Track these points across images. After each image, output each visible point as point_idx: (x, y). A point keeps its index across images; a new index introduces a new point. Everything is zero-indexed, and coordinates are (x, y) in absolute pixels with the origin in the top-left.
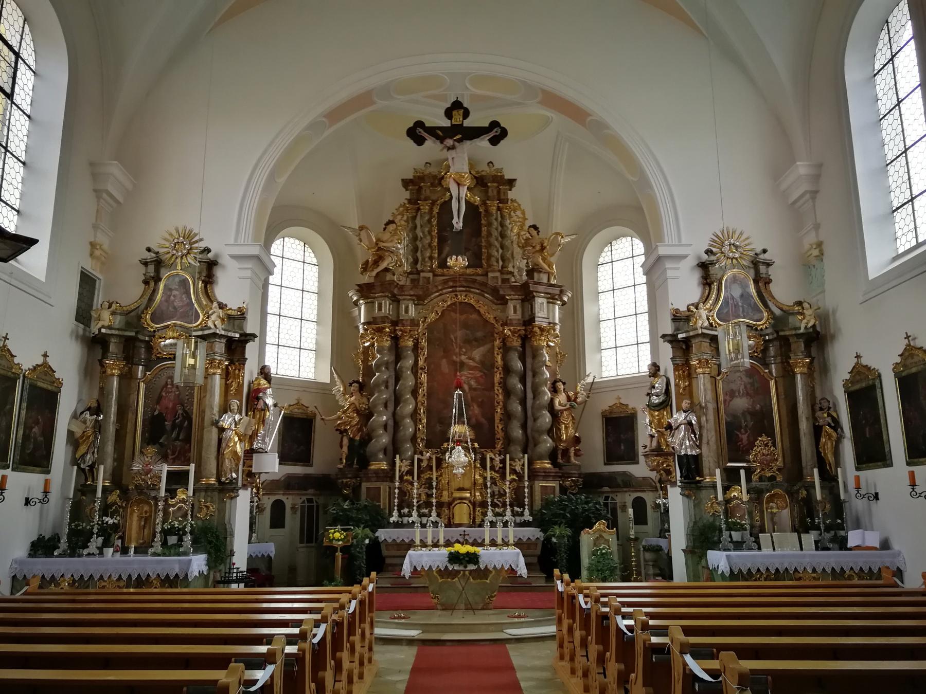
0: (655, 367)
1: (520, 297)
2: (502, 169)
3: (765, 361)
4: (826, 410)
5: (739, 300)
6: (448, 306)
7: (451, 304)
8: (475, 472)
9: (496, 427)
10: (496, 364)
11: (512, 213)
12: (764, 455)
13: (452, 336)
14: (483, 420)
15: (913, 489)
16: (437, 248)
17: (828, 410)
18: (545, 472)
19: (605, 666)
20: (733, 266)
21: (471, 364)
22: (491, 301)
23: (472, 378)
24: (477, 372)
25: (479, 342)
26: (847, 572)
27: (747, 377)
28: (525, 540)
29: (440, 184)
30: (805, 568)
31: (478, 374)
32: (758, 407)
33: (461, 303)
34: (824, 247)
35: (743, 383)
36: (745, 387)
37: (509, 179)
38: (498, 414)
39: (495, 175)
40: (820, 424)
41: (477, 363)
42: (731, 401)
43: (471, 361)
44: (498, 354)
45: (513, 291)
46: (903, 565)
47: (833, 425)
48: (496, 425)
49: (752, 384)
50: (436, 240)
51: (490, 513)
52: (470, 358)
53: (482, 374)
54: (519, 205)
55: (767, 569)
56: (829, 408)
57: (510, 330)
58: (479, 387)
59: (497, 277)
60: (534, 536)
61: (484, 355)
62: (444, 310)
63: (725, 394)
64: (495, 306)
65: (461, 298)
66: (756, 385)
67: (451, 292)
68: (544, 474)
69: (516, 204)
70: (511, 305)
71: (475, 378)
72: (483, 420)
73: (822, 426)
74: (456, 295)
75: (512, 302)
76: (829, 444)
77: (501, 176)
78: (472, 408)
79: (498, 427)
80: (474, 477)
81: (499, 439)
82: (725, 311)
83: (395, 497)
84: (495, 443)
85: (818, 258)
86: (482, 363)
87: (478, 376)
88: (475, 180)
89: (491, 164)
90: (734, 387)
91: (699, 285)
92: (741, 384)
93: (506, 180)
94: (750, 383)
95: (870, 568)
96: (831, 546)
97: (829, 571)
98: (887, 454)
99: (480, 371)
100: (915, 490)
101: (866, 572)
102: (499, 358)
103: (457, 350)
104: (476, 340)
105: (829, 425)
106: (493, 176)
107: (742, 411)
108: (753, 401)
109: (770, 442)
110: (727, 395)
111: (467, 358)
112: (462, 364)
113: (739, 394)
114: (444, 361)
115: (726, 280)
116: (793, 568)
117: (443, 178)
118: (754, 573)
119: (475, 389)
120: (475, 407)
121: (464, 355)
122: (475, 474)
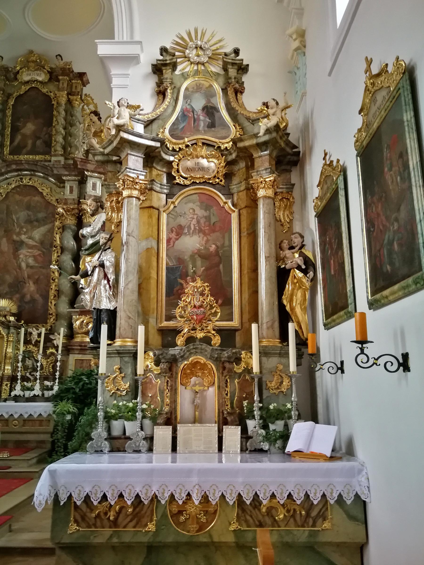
0: (97, 202)
1: (76, 178)
2: (71, 62)
3: (229, 189)
4: (297, 248)
5: (200, 112)
6: (13, 189)
7: (15, 187)
8: (7, 346)
9: (49, 304)
10: (55, 243)
11: (85, 107)
12: (195, 306)
13: (14, 217)
14: (37, 296)
15: (362, 350)
16: (9, 136)
17: (301, 248)
18: (80, 346)
19: (344, 459)
20: (197, 72)
21: (31, 243)
22: (55, 184)
23: (30, 256)
24: (35, 251)
25: (40, 222)
26: (265, 502)
27: (201, 209)
28: (36, 416)
29: (16, 79)
30: (189, 495)
31: (36, 252)
32: (213, 248)
33: (25, 186)
34: (309, 38)
35: (195, 217)
36: (198, 222)
37: (78, 73)
38: (53, 291)
39: (64, 68)
40: (288, 267)
41: (36, 242)
42: (177, 239)
43: (30, 240)
44: (56, 234)
45: (67, 171)
46: (366, 492)
47: (303, 267)
48: (50, 301)
49: (208, 218)
50: (10, 130)
51: (18, 387)
52: (30, 238)
53: (40, 252)
54: (92, 100)
55: (121, 496)
56: (303, 246)
57: (64, 209)
58: (37, 265)
59: (59, 161)
60: (45, 412)
61: (45, 235)
62: (8, 193)
63: (170, 230)
64: (58, 189)
65: (25, 181)
66: (213, 220)
67: (18, 176)
68: (79, 348)
69: (89, 99)
70: (67, 186)
71: (34, 257)
72: (37, 296)
73: (289, 270)
74: (21, 179)
75: (69, 182)
76: (299, 294)
77: (69, 69)
78: (28, 285)
79: (51, 303)
80: (6, 350)
81: (52, 314)
82: (181, 126)
83: (57, 370)
84: (47, 319)
85: (299, 51)
86: (42, 243)
87: (36, 254)
88: (48, 75)
89: (58, 57)
90: (183, 221)
91: (152, 96)
92: (193, 218)
93: (75, 73)
94: (206, 217)
95: (307, 496)
96: (266, 446)
97: (231, 499)
98: (349, 294)
99: (39, 250)
100: (365, 352)
101: (299, 502)
102: (58, 237)
103: (18, 230)
104: (37, 221)
105: (299, 268)
106: (61, 69)
107: (191, 253)
108: (207, 241)
109: (207, 289)
110: (172, 231)
111: (27, 238)
112: (22, 243)
113: (189, 231)
114: (4, 240)
115: (187, 89)
116: (167, 495)
117: (18, 72)
118: (95, 503)
119: (32, 267)
120: (31, 283)
121: (24, 234)
122: (7, 348)
